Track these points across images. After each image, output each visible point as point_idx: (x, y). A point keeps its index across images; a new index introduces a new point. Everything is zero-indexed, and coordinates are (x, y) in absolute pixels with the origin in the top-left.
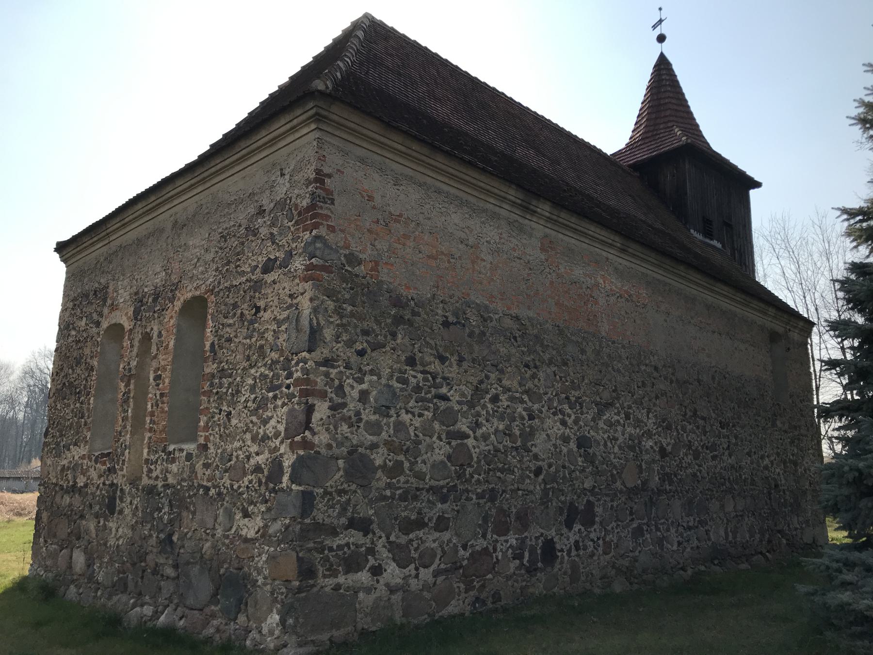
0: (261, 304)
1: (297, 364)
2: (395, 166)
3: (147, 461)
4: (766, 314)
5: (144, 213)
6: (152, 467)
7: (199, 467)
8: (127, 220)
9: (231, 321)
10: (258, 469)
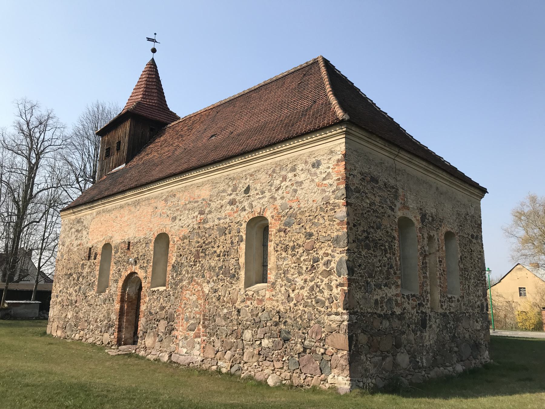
5: (424, 168)
6: (443, 304)
8: (413, 161)
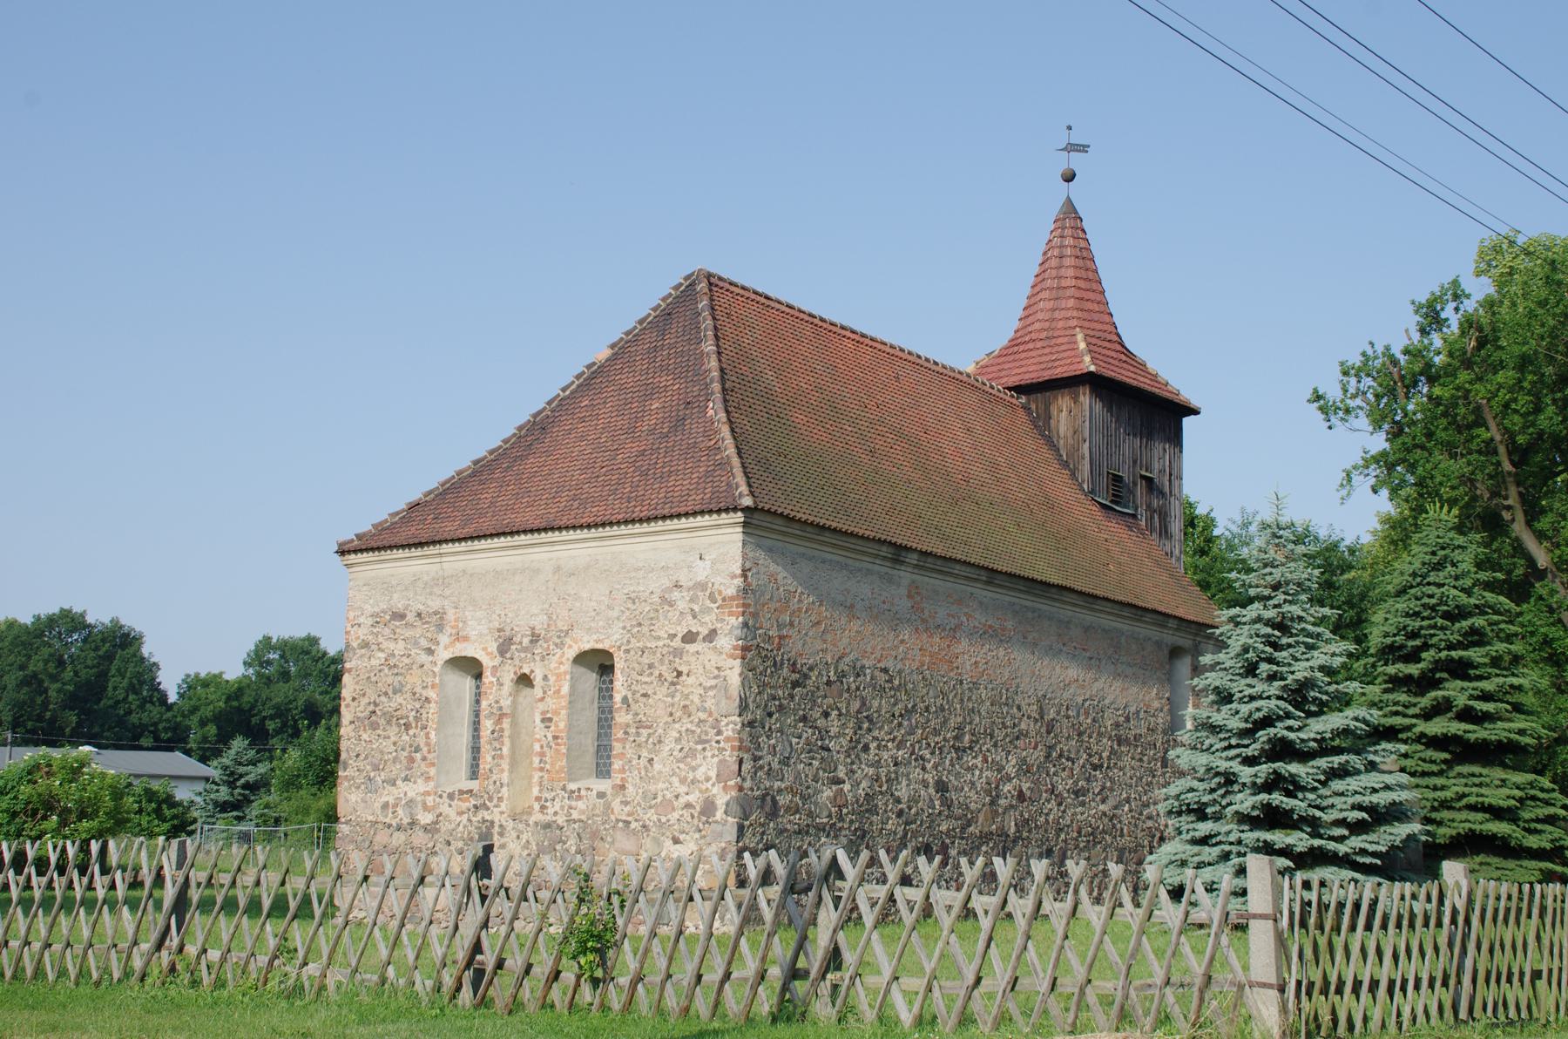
0: (684, 669)
1: (727, 724)
2: (792, 547)
3: (538, 799)
4: (1165, 627)
7: (616, 804)
9: (647, 679)
10: (688, 806)
